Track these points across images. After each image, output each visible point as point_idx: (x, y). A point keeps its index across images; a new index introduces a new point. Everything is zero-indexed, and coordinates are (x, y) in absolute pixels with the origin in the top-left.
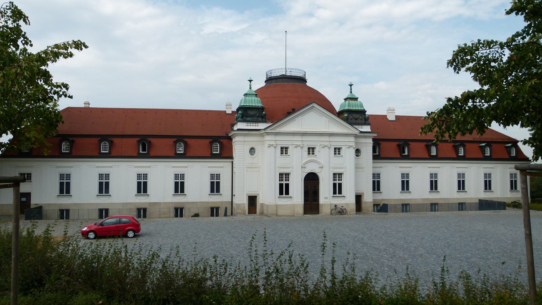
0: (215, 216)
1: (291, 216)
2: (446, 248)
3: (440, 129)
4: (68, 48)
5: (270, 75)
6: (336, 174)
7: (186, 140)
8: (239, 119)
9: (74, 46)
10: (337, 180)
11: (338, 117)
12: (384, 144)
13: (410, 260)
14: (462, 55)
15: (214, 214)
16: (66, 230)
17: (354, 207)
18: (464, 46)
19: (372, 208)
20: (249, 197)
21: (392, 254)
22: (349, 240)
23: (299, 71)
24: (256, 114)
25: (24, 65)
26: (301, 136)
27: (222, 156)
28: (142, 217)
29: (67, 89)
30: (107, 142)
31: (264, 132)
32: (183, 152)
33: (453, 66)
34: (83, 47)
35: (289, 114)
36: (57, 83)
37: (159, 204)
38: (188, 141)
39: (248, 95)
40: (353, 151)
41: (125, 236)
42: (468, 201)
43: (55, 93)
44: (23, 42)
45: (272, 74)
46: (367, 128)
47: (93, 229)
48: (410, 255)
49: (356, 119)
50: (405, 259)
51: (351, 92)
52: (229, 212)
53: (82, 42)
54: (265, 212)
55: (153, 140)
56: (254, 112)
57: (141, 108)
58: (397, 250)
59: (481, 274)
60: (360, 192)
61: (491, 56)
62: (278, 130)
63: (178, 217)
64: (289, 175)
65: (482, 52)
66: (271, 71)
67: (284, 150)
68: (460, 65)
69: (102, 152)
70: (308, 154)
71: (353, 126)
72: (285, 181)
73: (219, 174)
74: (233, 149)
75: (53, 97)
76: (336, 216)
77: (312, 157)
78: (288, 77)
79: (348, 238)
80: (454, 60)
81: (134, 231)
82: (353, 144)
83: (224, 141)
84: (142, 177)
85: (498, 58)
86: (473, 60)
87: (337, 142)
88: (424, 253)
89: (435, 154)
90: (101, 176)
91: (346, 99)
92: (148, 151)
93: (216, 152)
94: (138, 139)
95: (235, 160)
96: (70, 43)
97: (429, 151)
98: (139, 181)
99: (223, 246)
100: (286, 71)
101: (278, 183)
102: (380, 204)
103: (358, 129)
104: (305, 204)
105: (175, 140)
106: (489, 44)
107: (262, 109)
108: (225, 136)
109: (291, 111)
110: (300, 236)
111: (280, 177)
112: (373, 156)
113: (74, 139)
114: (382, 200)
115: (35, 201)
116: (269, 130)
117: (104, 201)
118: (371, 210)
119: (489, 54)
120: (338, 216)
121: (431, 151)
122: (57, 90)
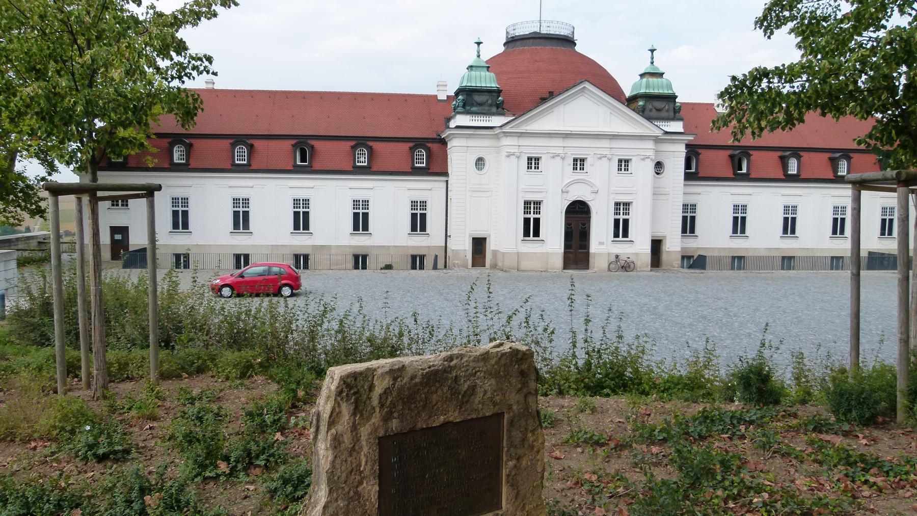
0: (418, 268)
1: (542, 271)
2: (793, 326)
3: (739, 121)
4: (211, 5)
6: (620, 204)
7: (370, 143)
8: (459, 109)
10: (621, 214)
11: (628, 106)
12: (705, 154)
13: (728, 342)
14: (778, 10)
15: (416, 266)
16: (195, 275)
17: (648, 259)
19: (680, 262)
20: (474, 239)
21: (701, 331)
22: (633, 310)
24: (487, 101)
25: (154, 32)
26: (608, 140)
27: (430, 171)
28: (302, 268)
29: (211, 63)
30: (244, 147)
31: (500, 131)
32: (366, 164)
33: (763, 27)
34: (231, 4)
35: (544, 100)
36: (196, 54)
37: (329, 247)
38: (376, 145)
39: (473, 68)
40: (651, 166)
41: (278, 293)
42: (750, 254)
43: (194, 68)
45: (516, 31)
47: (227, 282)
48: (730, 334)
49: (659, 110)
50: (722, 340)
51: (652, 63)
54: (500, 264)
55: (317, 144)
56: (484, 97)
57: (283, 90)
58: (709, 326)
59: (823, 352)
60: (659, 234)
61: (821, 11)
62: (523, 129)
63: (359, 268)
64: (540, 205)
66: (514, 25)
67: (533, 162)
68: (773, 26)
69: (416, 165)
70: (574, 169)
71: (652, 122)
72: (534, 214)
73: (424, 200)
74: (449, 160)
75: (191, 74)
76: (617, 273)
77: (579, 175)
78: (543, 36)
79: (631, 306)
80: (765, 17)
81: (292, 287)
82: (651, 153)
83: (434, 146)
84: (301, 204)
85: (830, 16)
86: (793, 18)
87: (623, 149)
88: (754, 332)
90: (236, 201)
91: (642, 76)
92: (310, 162)
93: (420, 165)
94: (294, 142)
95: (452, 179)
97: (785, 167)
98: (236, 209)
99: (431, 313)
100: (540, 26)
102: (693, 256)
103: (661, 127)
104: (565, 252)
107: (498, 92)
109: (547, 95)
110: (553, 300)
111: (525, 207)
112: (686, 174)
113: (192, 141)
114: (698, 248)
116: (507, 128)
117: (242, 242)
118: (677, 266)
120: (621, 273)
122: (196, 64)
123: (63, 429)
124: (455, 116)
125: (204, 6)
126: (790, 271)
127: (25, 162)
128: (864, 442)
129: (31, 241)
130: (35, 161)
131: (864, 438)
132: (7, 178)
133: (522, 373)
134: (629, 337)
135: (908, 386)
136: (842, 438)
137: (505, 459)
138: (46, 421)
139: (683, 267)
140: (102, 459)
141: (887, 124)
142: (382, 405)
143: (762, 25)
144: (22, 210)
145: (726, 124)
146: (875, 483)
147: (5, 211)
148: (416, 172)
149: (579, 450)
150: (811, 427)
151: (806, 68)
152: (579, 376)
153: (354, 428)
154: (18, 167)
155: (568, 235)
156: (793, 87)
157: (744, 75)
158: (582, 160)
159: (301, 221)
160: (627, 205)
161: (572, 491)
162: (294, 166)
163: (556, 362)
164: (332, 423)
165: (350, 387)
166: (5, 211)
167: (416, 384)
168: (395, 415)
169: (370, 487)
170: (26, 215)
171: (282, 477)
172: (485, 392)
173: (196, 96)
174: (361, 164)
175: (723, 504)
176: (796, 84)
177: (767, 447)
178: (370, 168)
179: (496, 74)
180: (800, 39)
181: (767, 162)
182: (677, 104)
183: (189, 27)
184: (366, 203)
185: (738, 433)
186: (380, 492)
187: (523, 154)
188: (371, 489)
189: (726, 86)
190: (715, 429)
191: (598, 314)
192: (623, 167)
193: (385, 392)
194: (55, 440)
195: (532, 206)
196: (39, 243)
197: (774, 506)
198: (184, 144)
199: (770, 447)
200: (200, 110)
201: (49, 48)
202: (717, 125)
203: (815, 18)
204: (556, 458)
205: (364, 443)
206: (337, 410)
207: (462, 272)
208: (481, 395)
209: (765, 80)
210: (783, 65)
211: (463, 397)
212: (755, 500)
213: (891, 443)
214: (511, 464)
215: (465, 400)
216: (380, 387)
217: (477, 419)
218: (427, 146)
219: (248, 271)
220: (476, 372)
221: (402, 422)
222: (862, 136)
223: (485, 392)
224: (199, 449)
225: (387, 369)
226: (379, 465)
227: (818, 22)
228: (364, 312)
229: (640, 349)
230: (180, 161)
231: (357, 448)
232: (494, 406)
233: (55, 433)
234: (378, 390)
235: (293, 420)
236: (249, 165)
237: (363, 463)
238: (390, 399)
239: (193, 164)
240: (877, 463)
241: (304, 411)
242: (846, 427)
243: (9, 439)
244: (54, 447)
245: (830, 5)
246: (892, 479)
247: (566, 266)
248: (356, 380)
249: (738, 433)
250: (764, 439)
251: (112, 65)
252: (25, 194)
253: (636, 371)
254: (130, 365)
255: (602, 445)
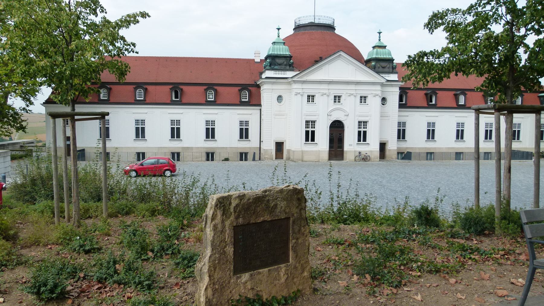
3: (416, 78)
4: (136, 17)
5: (298, 23)
7: (216, 87)
8: (268, 67)
9: (140, 15)
10: (310, 127)
11: (366, 65)
17: (378, 154)
18: (437, 12)
19: (396, 156)
20: (276, 143)
22: (368, 183)
23: (328, 19)
24: (284, 62)
26: (301, 84)
29: (135, 47)
32: (213, 99)
35: (317, 62)
37: (192, 148)
38: (218, 88)
40: (379, 100)
42: (437, 151)
43: (126, 50)
44: (101, 10)
46: (394, 77)
47: (133, 168)
49: (384, 68)
50: (418, 200)
51: (380, 40)
52: (257, 157)
53: (147, 12)
54: (292, 157)
55: (184, 88)
60: (384, 140)
62: (305, 79)
65: (450, 17)
66: (299, 18)
67: (311, 98)
69: (138, 99)
74: (262, 97)
75: (124, 53)
77: (338, 105)
80: (429, 23)
82: (379, 93)
83: (253, 89)
85: (462, 23)
86: (443, 24)
87: (364, 90)
89: (463, 103)
90: (137, 121)
91: (374, 47)
92: (181, 98)
94: (171, 87)
96: (138, 13)
97: (457, 100)
98: (207, 127)
101: (304, 130)
104: (330, 151)
105: (205, 87)
106: (454, 11)
107: (290, 57)
108: (254, 85)
109: (319, 59)
113: (111, 86)
114: (407, 148)
115: (80, 145)
117: (140, 146)
118: (394, 158)
119: (455, 19)
121: (459, 100)
123: (64, 239)
124: (265, 71)
125: (132, 17)
126: (460, 161)
127: (13, 99)
128: (475, 242)
129: (16, 145)
130: (19, 98)
131: (476, 240)
132: (3, 108)
133: (299, 199)
134: (362, 196)
135: (501, 215)
136: (465, 241)
137: (291, 239)
138: (55, 235)
139: (398, 158)
140: (87, 252)
141: (490, 80)
142: (235, 212)
143: (428, 26)
144: (11, 127)
145: (409, 79)
146: (474, 258)
147: (2, 127)
148: (243, 104)
149: (330, 247)
150: (449, 236)
151: (446, 50)
152: (334, 216)
153: (223, 222)
154: (10, 102)
155: (331, 141)
156: (440, 61)
157: (415, 55)
158: (339, 97)
159: (175, 133)
160: (365, 123)
161: (326, 264)
162: (171, 101)
163: (322, 209)
164: (213, 219)
165: (221, 203)
166: (2, 127)
167: (250, 203)
168: (241, 216)
169: (230, 249)
170: (13, 130)
171: (182, 257)
172: (282, 207)
173: (127, 65)
174: (210, 100)
175: (398, 268)
176: (441, 60)
177: (425, 244)
178: (216, 102)
179: (289, 47)
180: (448, 34)
181: (446, 98)
182: (394, 64)
183: (124, 28)
184: (213, 122)
185: (412, 238)
186: (234, 251)
187: (305, 93)
188: (230, 250)
189: (406, 60)
190: (400, 236)
191: (345, 184)
192: (311, 100)
193: (236, 206)
194: (61, 244)
195: (311, 123)
196: (21, 146)
197: (423, 268)
198: (107, 88)
199: (427, 244)
200: (128, 72)
201: (51, 40)
202: (405, 80)
203: (455, 24)
204: (319, 251)
205: (227, 229)
206: (215, 213)
207: (270, 162)
208: (280, 208)
209: (426, 57)
210: (435, 50)
211: (271, 209)
212: (414, 265)
213: (489, 243)
214: (294, 241)
215: (272, 210)
216: (234, 203)
217: (278, 220)
218: (249, 89)
219: (146, 162)
220: (277, 198)
221: (244, 219)
222: (479, 86)
223: (282, 207)
224: (138, 246)
225: (237, 196)
226: (234, 239)
227: (456, 26)
228: (215, 183)
229: (368, 202)
230: (104, 98)
231: (224, 230)
232: (286, 214)
233: (60, 241)
234: (233, 205)
235: (183, 234)
236: (145, 100)
237: (227, 238)
238: (238, 209)
239: (112, 100)
240: (478, 250)
241: (187, 231)
242: (467, 235)
243: (37, 244)
244: (61, 247)
245: (462, 17)
246: (483, 257)
247: (330, 158)
248: (223, 200)
249: (412, 238)
250: (424, 241)
251: (86, 50)
252: (14, 118)
253: (366, 213)
254: (90, 210)
255: (342, 244)
